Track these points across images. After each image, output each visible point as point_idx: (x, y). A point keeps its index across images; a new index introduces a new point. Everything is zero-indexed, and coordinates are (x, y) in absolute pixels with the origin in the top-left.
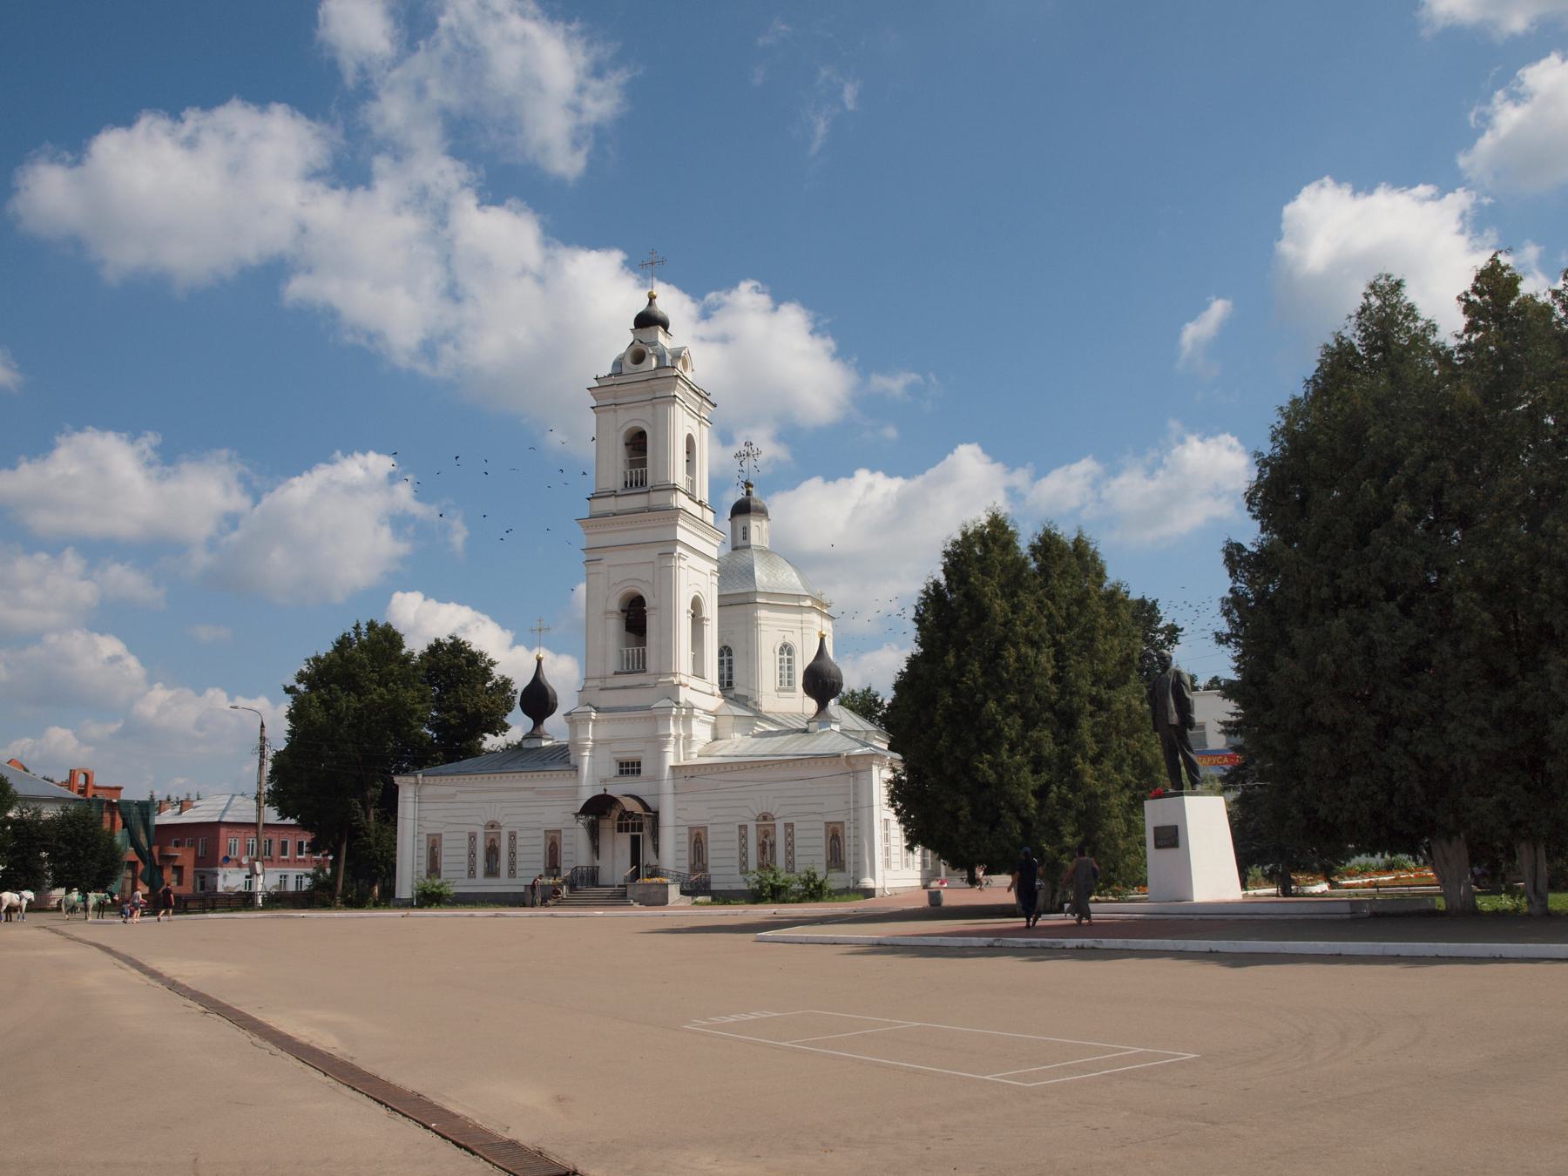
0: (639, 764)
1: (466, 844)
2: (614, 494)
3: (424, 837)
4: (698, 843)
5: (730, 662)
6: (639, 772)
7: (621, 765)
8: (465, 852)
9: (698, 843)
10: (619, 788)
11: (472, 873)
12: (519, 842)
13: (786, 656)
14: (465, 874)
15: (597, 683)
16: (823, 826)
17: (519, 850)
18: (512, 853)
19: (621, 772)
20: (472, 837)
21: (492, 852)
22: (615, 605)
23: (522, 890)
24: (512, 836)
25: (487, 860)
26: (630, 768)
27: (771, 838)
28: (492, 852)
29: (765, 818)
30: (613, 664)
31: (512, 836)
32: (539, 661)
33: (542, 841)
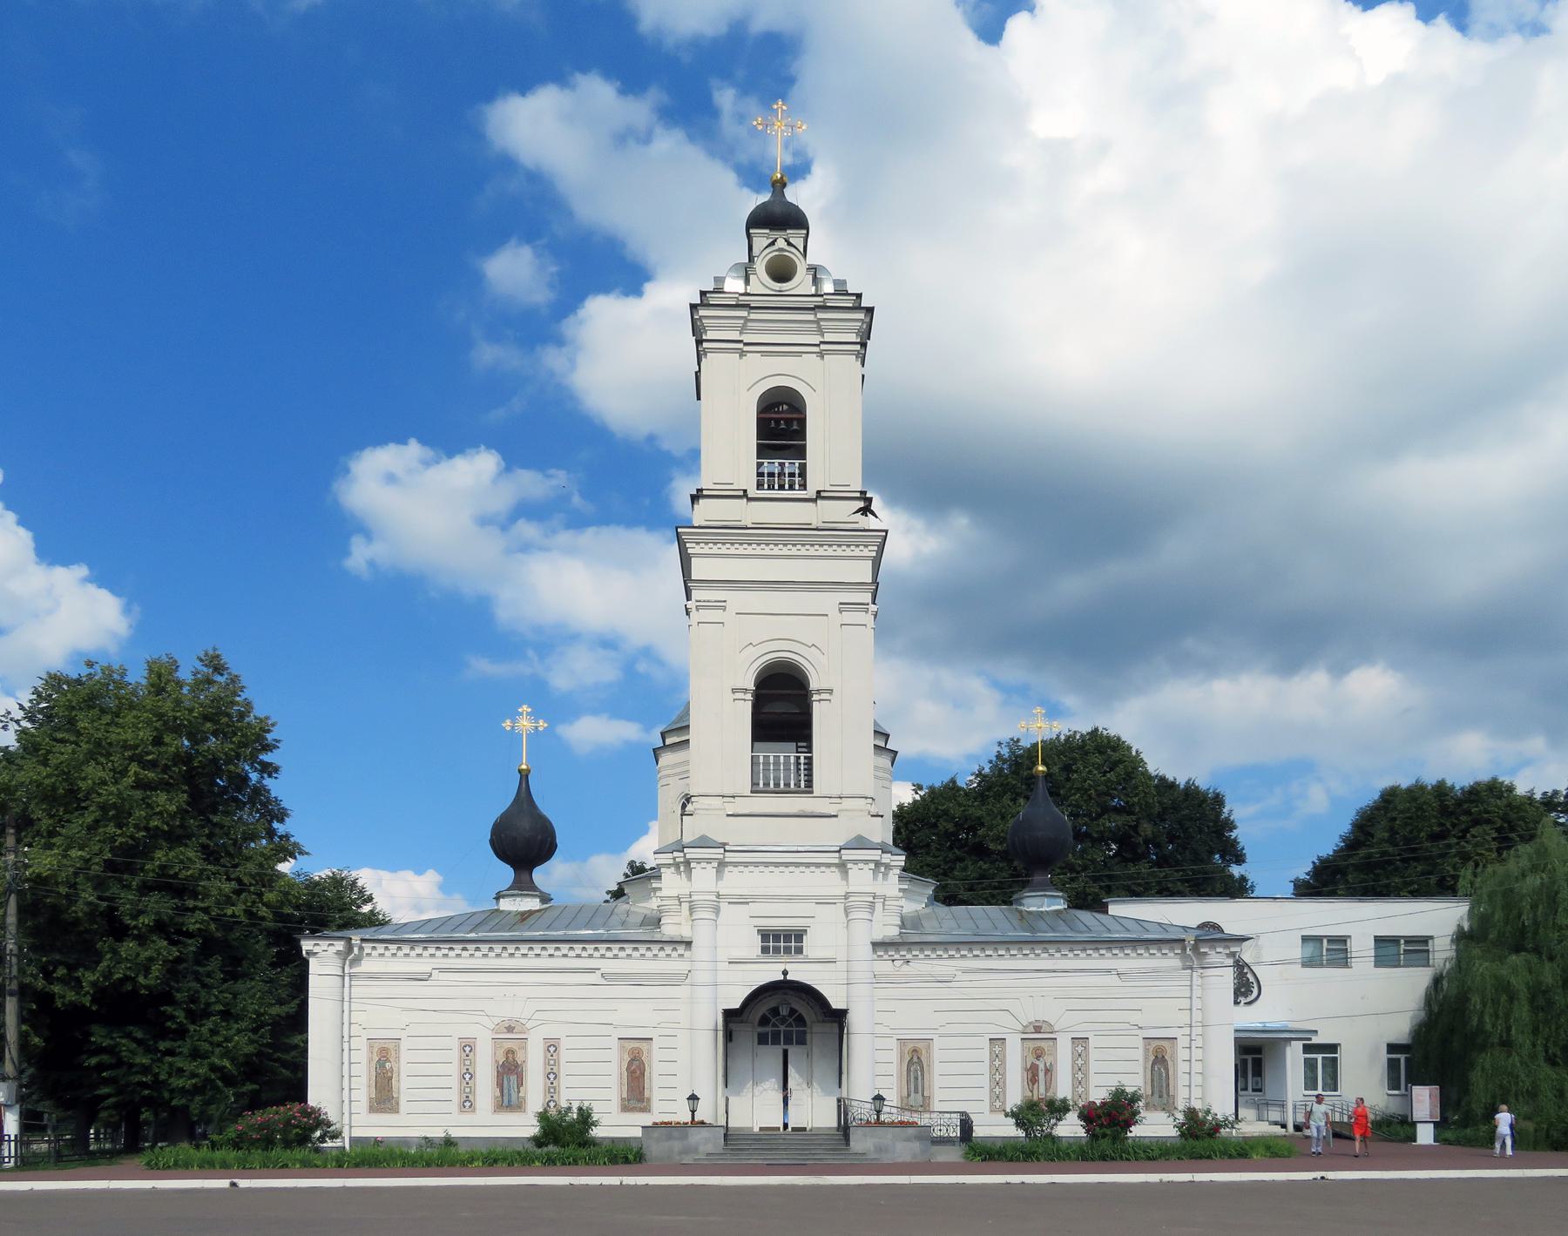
3: (360, 1044)
4: (915, 1063)
6: (799, 950)
9: (915, 1063)
11: (467, 1104)
16: (1140, 1043)
17: (564, 1070)
19: (765, 950)
20: (468, 1047)
23: (638, 1133)
24: (552, 1046)
25: (500, 1085)
27: (1048, 1059)
29: (510, 1029)
31: (552, 1046)
32: (524, 776)
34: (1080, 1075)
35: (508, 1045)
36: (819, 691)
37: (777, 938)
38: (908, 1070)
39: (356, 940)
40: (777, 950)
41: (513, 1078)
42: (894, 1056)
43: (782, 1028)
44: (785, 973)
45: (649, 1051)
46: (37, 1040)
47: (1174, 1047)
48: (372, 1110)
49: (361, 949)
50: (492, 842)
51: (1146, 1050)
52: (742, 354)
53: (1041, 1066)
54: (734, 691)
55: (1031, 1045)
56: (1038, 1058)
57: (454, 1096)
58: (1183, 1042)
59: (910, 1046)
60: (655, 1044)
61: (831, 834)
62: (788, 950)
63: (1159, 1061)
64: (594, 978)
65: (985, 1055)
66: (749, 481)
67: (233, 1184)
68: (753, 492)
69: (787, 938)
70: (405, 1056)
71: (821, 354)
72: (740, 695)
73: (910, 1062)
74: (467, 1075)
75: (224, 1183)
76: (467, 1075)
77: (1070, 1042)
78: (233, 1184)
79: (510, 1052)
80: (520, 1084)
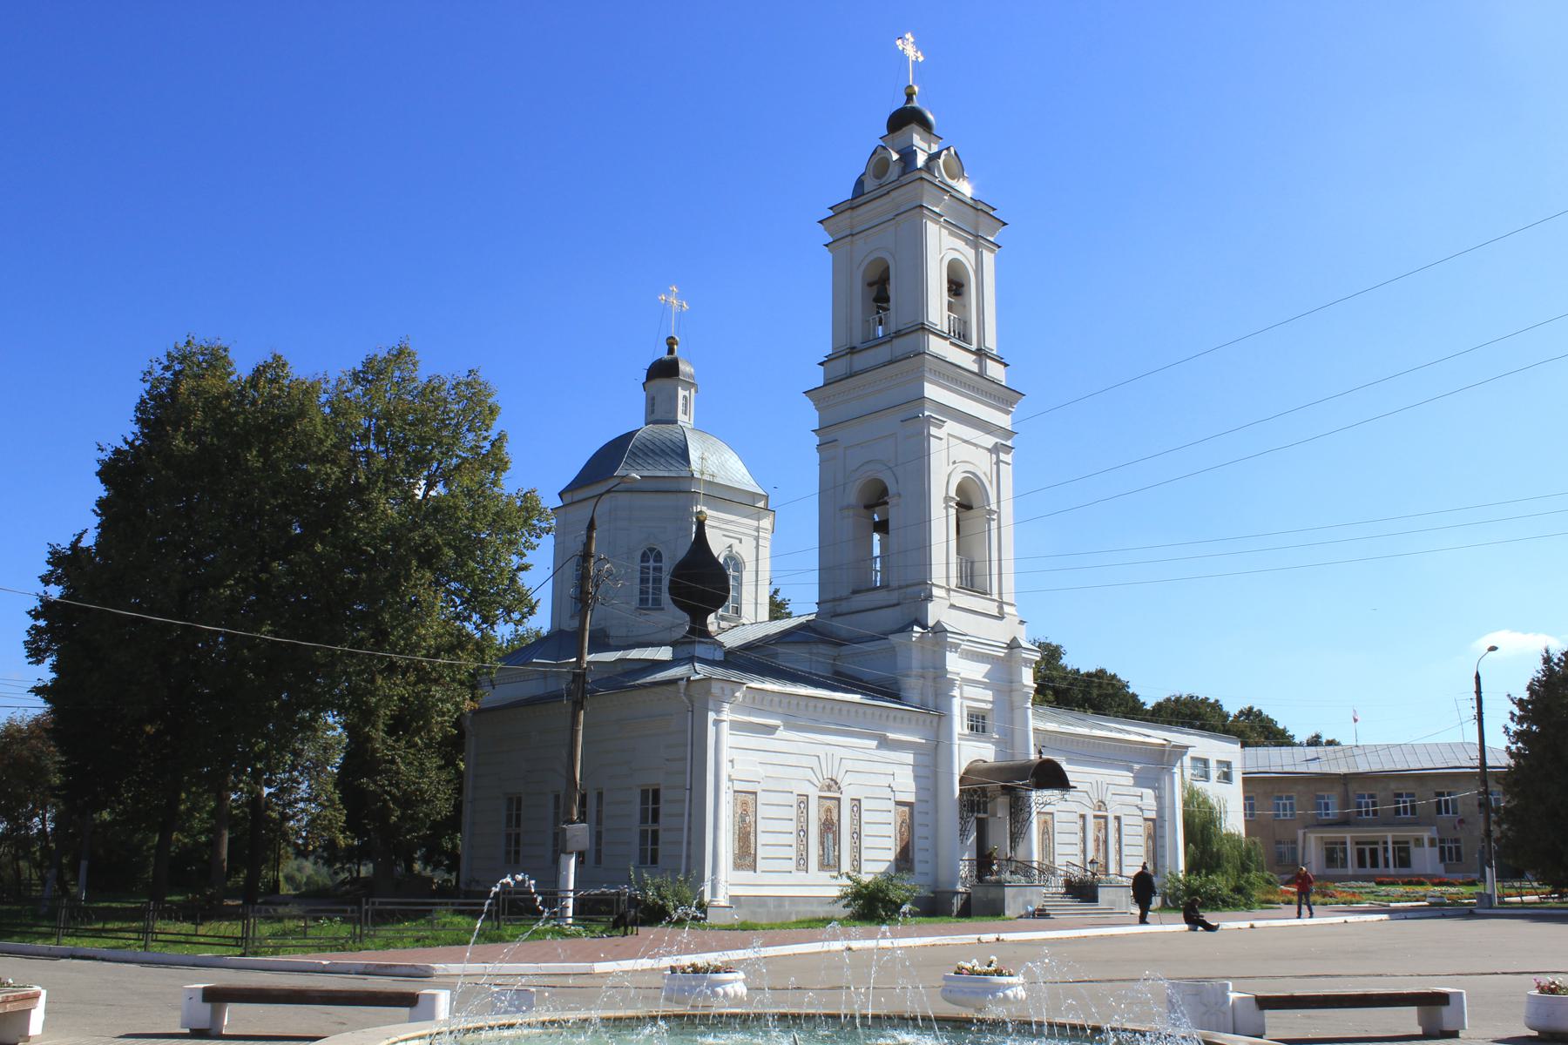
2: (853, 350)
11: (802, 863)
13: (651, 564)
14: (792, 865)
18: (857, 835)
21: (829, 827)
24: (857, 802)
25: (822, 843)
28: (829, 827)
29: (829, 788)
48: (738, 866)
70: (762, 811)
74: (804, 832)
76: (804, 832)
79: (829, 810)
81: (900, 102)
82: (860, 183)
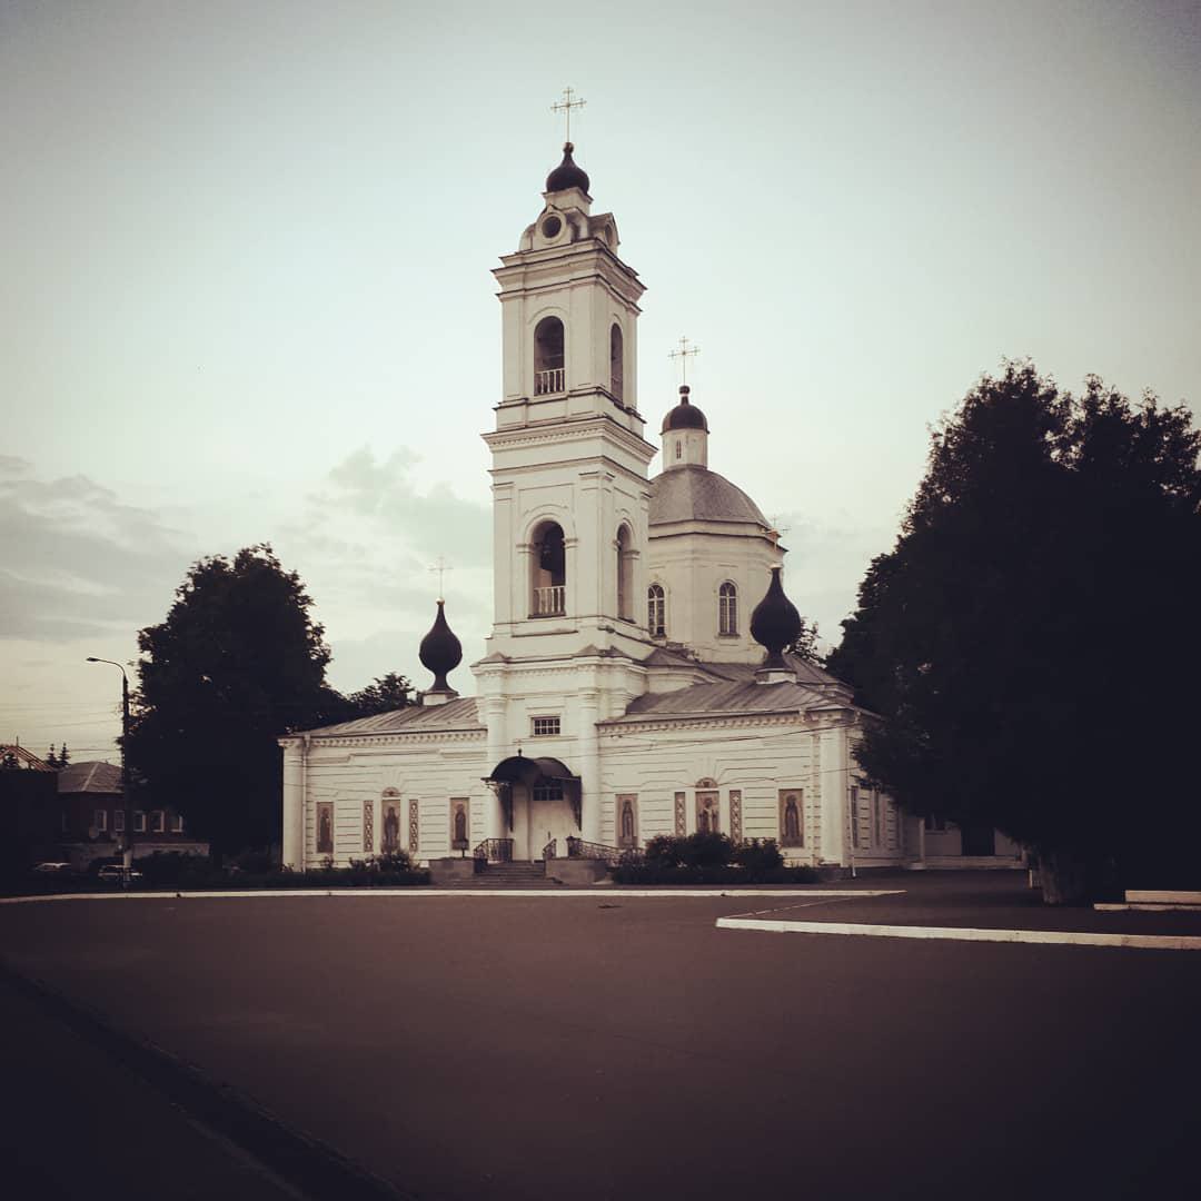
0: (558, 722)
1: (361, 813)
2: (526, 403)
3: (313, 806)
4: (627, 809)
5: (733, 602)
6: (558, 731)
7: (537, 723)
8: (361, 822)
9: (627, 809)
10: (537, 749)
12: (421, 812)
15: (507, 628)
17: (421, 820)
18: (414, 823)
19: (537, 732)
20: (368, 805)
22: (525, 535)
24: (414, 804)
26: (547, 726)
27: (714, 807)
29: (391, 794)
30: (523, 607)
31: (414, 804)
33: (447, 810)
34: (736, 820)
35: (391, 804)
36: (569, 541)
37: (544, 723)
38: (786, 815)
39: (307, 737)
40: (544, 731)
41: (393, 827)
42: (775, 802)
43: (548, 788)
44: (520, 751)
45: (468, 808)
46: (925, 666)
47: (801, 795)
49: (311, 742)
50: (420, 655)
51: (781, 799)
52: (524, 297)
53: (710, 812)
54: (519, 546)
55: (703, 797)
56: (707, 807)
57: (360, 839)
58: (806, 792)
59: (788, 794)
60: (472, 801)
61: (572, 645)
62: (551, 731)
63: (791, 806)
64: (433, 758)
65: (671, 804)
66: (530, 393)
67: (178, 895)
68: (532, 399)
69: (551, 723)
70: (337, 813)
71: (572, 288)
72: (521, 550)
73: (624, 812)
74: (368, 825)
75: (173, 895)
76: (368, 825)
77: (694, 794)
78: (178, 895)
80: (397, 831)
81: (556, 161)
82: (531, 231)
